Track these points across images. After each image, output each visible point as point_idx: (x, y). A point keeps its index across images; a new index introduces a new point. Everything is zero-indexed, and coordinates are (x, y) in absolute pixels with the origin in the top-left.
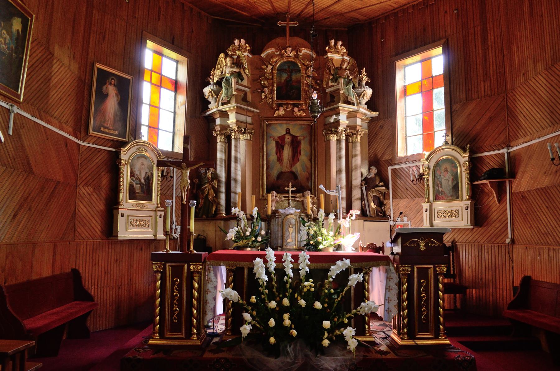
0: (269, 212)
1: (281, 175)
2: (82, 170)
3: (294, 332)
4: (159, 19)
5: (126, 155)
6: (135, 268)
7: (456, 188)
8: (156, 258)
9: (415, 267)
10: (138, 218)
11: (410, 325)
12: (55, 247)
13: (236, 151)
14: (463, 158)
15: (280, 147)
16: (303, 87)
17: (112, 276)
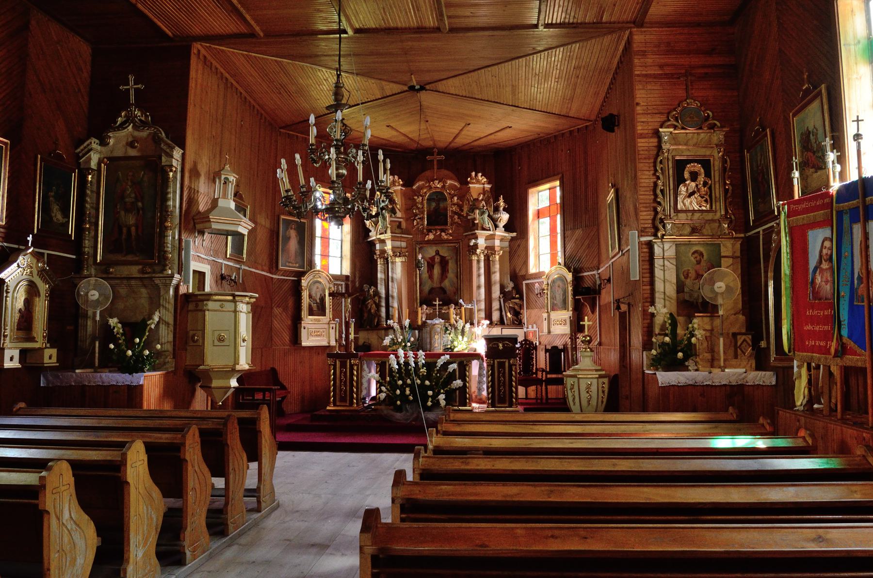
0: (420, 323)
1: (432, 290)
3: (411, 398)
5: (304, 283)
7: (565, 301)
8: (330, 356)
9: (496, 362)
11: (493, 398)
13: (393, 272)
14: (569, 276)
15: (431, 266)
16: (449, 214)
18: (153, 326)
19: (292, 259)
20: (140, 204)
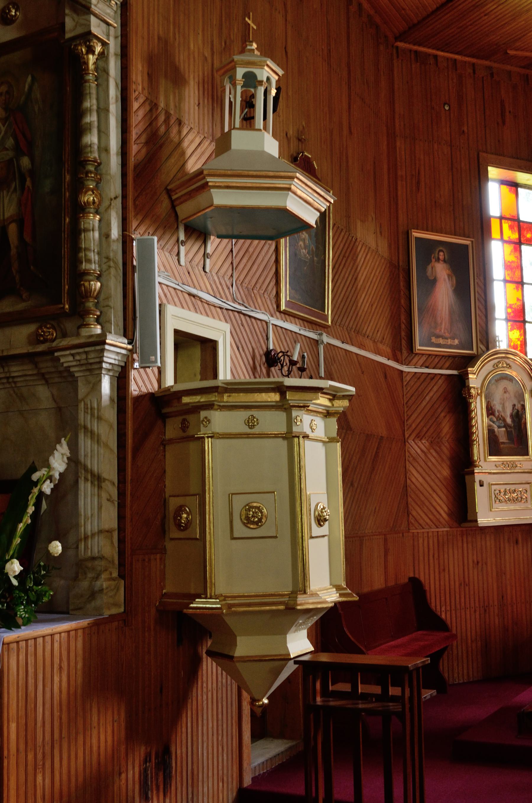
2: (409, 413)
4: (504, 123)
5: (475, 379)
6: (508, 577)
10: (508, 487)
12: (386, 540)
17: (472, 588)
18: (47, 488)
19: (444, 327)
20: (25, 161)
